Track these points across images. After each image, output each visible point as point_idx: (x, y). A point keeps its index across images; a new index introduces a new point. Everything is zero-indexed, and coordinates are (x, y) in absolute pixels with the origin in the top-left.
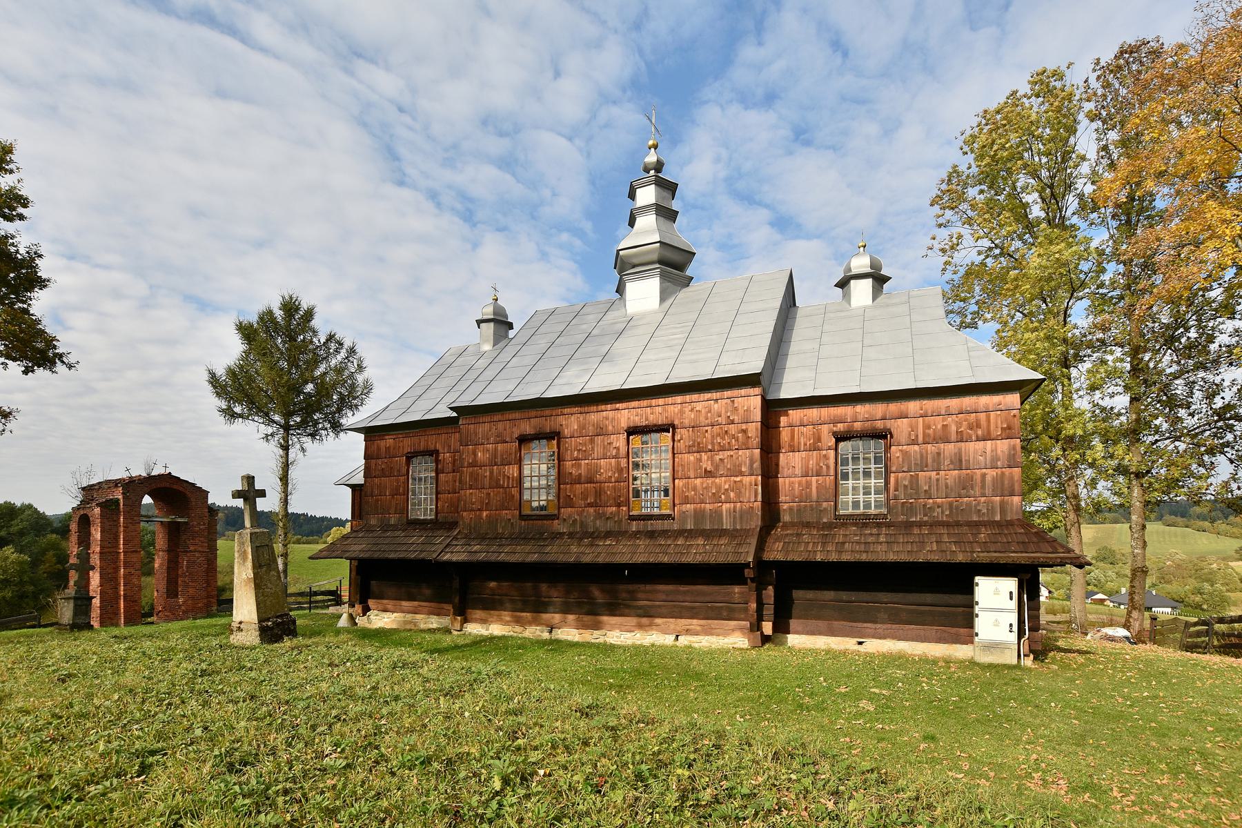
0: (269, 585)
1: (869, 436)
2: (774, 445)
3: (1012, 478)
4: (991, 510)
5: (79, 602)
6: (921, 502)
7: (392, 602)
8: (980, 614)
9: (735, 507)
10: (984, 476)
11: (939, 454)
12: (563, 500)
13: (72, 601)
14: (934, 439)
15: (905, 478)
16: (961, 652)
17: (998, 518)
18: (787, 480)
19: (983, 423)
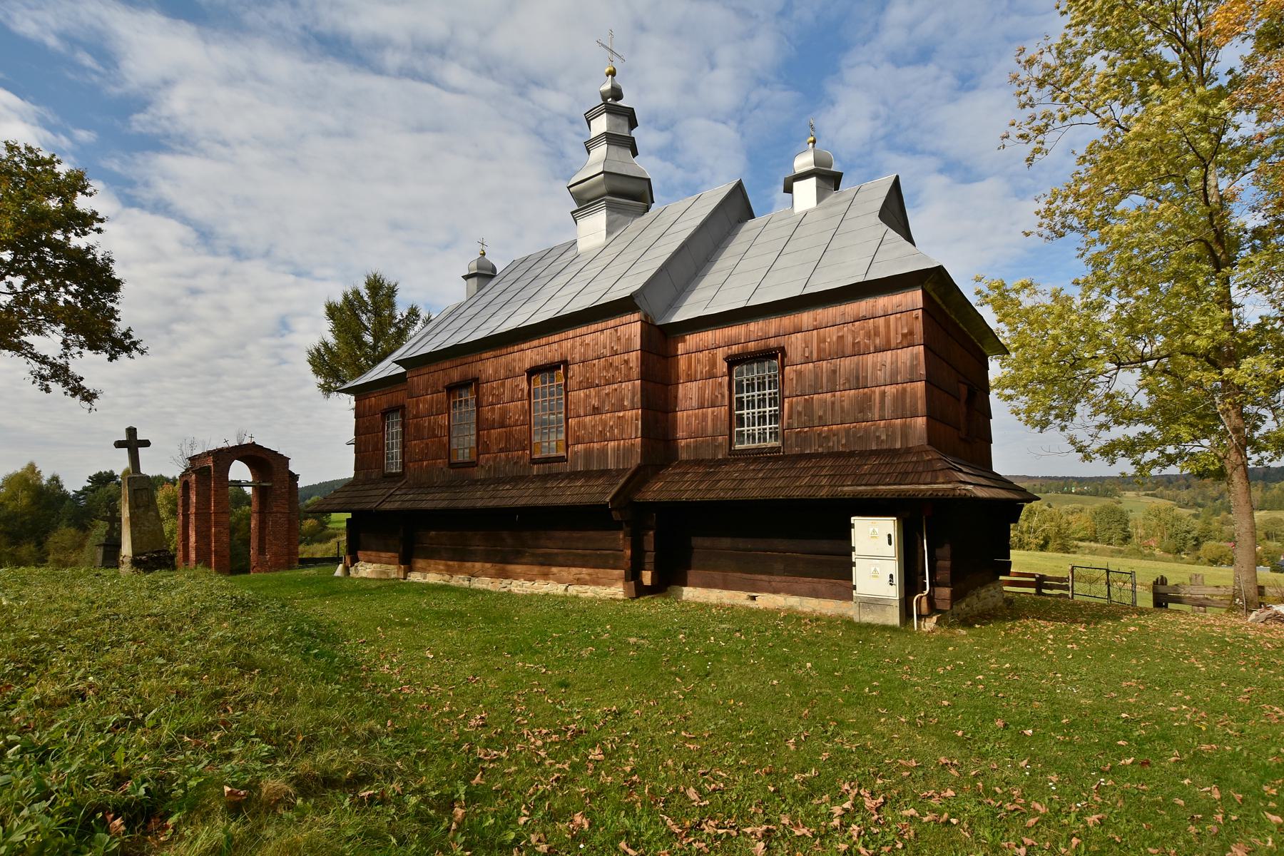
0: (146, 524)
1: (763, 357)
2: (673, 377)
3: (914, 394)
4: (892, 437)
5: (108, 549)
6: (817, 430)
7: (374, 553)
8: (858, 562)
9: (619, 445)
10: (883, 394)
11: (834, 372)
12: (482, 446)
13: (102, 548)
14: (830, 355)
15: (797, 403)
16: (829, 607)
17: (898, 446)
18: (685, 413)
19: (882, 329)
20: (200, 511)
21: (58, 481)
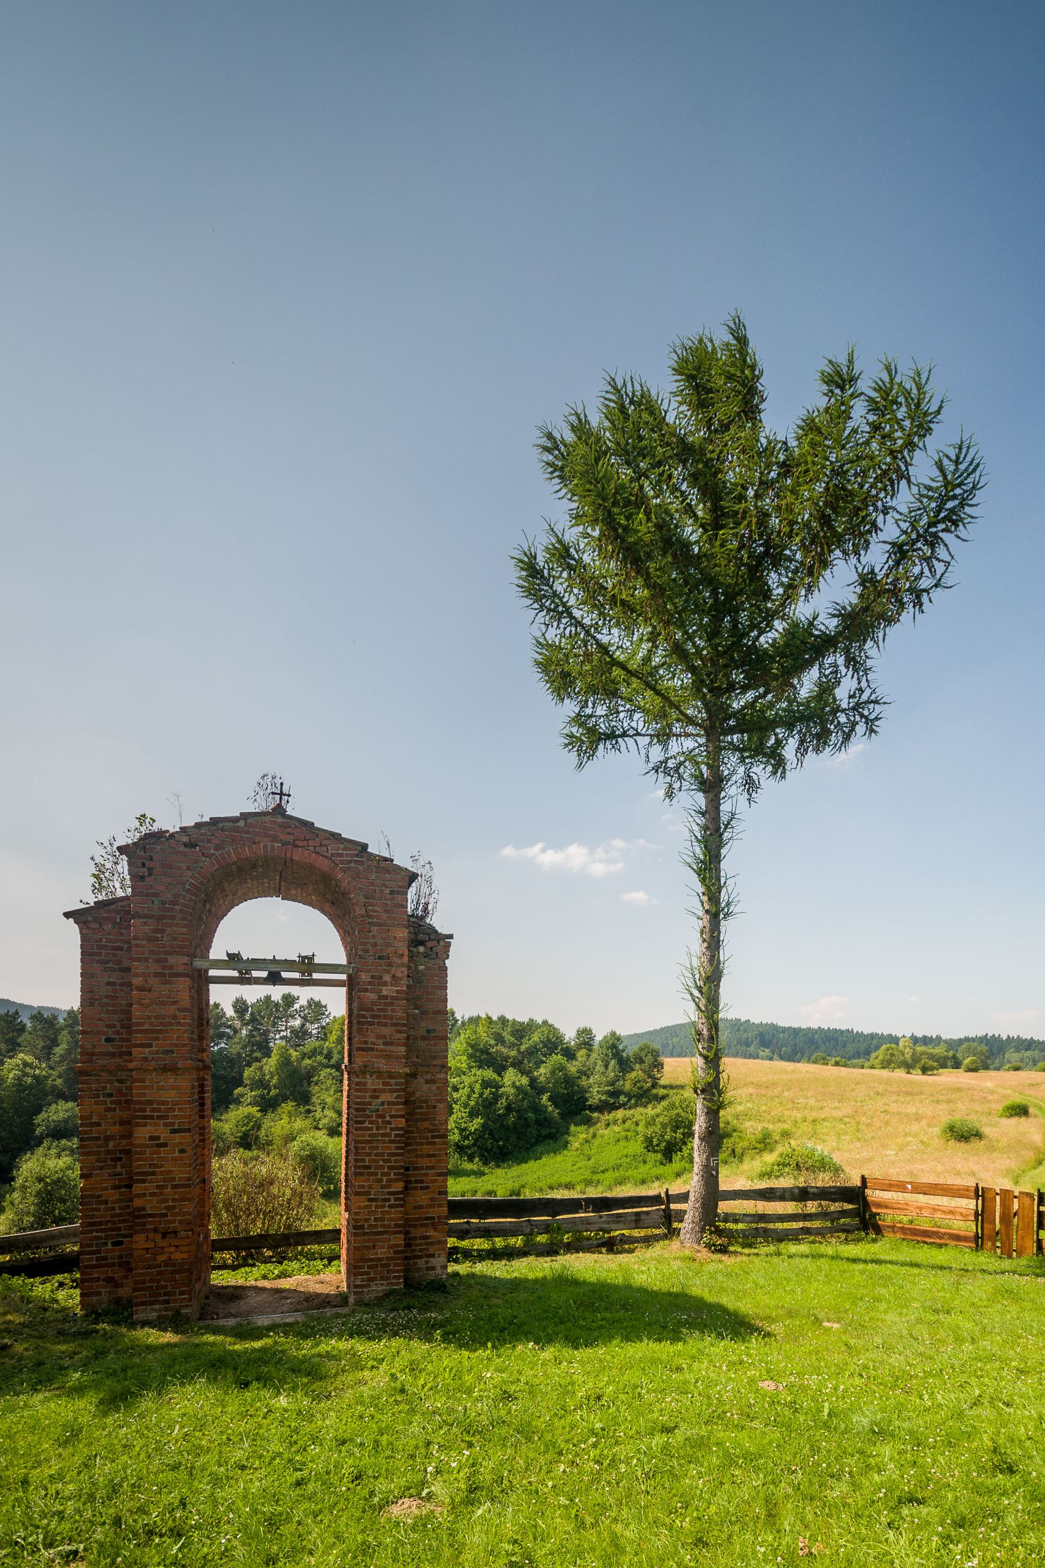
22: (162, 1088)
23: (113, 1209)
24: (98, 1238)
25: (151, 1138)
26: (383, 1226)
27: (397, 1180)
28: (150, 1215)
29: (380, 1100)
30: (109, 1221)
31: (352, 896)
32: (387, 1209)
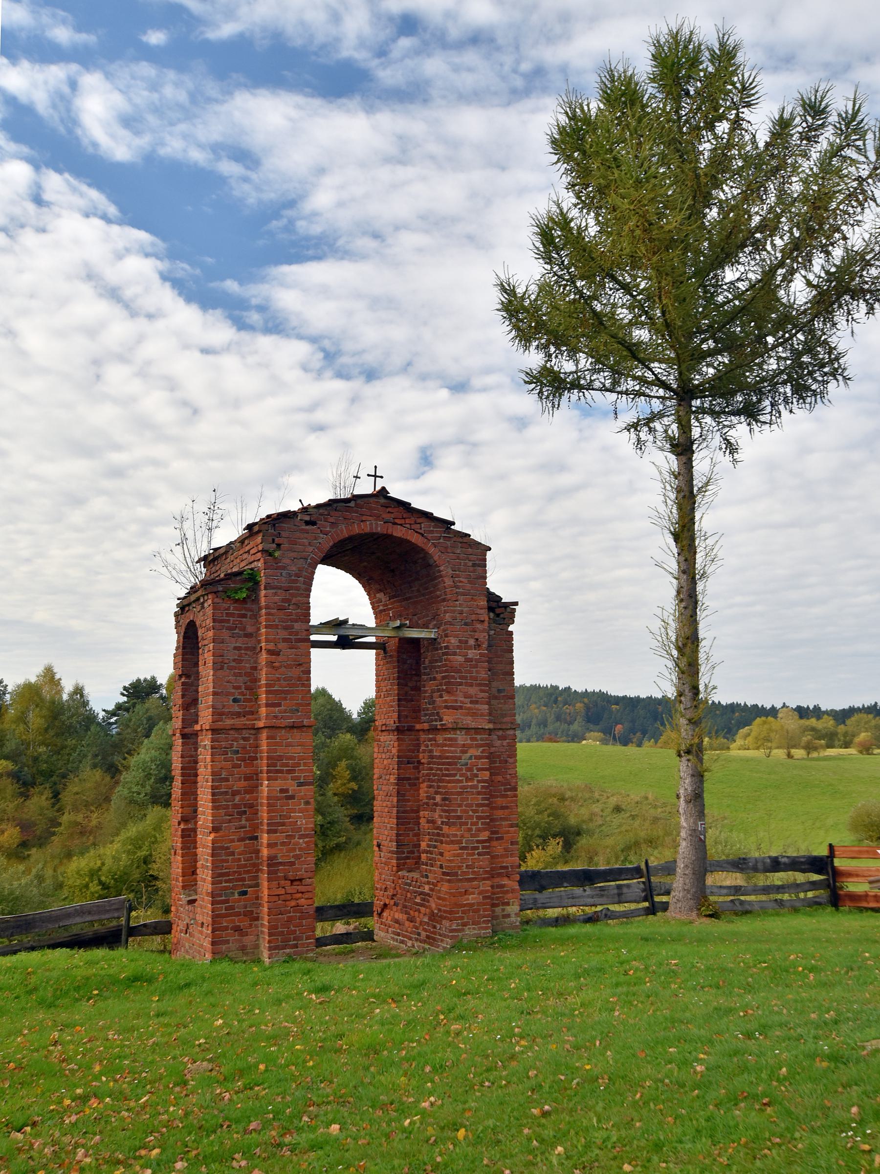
20: (229, 722)
21: (82, 696)
22: (289, 745)
23: (239, 860)
24: (227, 888)
25: (282, 791)
26: (474, 873)
27: (485, 830)
28: (281, 864)
29: (469, 755)
30: (236, 872)
31: (442, 568)
32: (476, 856)
